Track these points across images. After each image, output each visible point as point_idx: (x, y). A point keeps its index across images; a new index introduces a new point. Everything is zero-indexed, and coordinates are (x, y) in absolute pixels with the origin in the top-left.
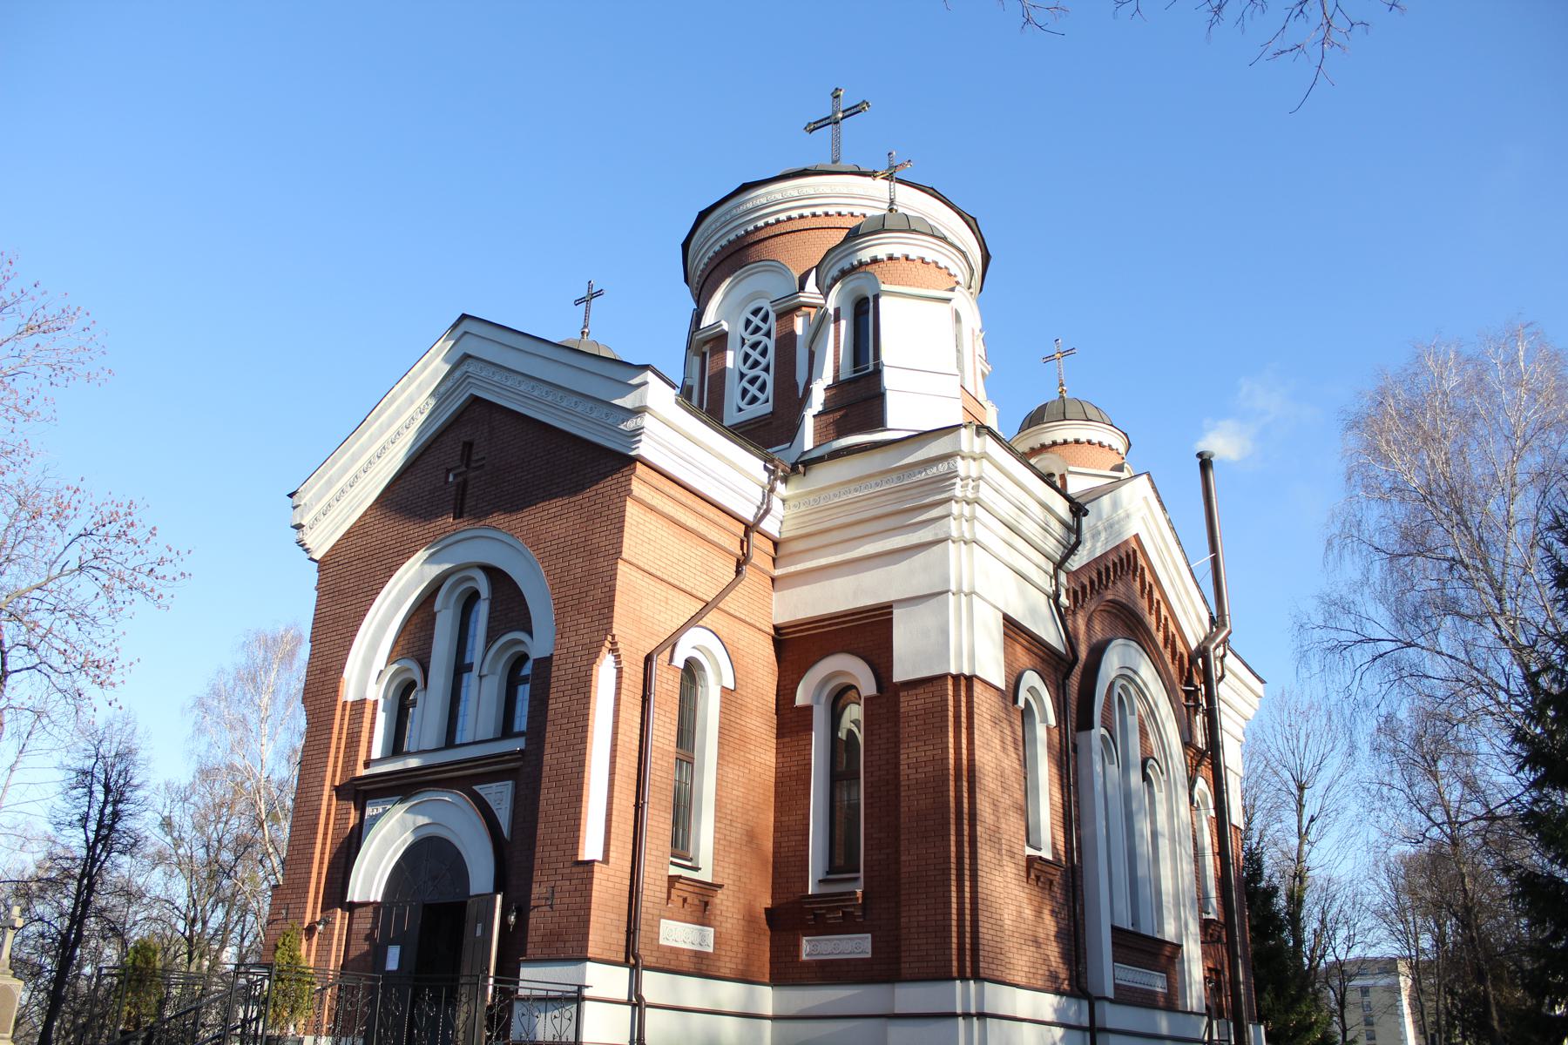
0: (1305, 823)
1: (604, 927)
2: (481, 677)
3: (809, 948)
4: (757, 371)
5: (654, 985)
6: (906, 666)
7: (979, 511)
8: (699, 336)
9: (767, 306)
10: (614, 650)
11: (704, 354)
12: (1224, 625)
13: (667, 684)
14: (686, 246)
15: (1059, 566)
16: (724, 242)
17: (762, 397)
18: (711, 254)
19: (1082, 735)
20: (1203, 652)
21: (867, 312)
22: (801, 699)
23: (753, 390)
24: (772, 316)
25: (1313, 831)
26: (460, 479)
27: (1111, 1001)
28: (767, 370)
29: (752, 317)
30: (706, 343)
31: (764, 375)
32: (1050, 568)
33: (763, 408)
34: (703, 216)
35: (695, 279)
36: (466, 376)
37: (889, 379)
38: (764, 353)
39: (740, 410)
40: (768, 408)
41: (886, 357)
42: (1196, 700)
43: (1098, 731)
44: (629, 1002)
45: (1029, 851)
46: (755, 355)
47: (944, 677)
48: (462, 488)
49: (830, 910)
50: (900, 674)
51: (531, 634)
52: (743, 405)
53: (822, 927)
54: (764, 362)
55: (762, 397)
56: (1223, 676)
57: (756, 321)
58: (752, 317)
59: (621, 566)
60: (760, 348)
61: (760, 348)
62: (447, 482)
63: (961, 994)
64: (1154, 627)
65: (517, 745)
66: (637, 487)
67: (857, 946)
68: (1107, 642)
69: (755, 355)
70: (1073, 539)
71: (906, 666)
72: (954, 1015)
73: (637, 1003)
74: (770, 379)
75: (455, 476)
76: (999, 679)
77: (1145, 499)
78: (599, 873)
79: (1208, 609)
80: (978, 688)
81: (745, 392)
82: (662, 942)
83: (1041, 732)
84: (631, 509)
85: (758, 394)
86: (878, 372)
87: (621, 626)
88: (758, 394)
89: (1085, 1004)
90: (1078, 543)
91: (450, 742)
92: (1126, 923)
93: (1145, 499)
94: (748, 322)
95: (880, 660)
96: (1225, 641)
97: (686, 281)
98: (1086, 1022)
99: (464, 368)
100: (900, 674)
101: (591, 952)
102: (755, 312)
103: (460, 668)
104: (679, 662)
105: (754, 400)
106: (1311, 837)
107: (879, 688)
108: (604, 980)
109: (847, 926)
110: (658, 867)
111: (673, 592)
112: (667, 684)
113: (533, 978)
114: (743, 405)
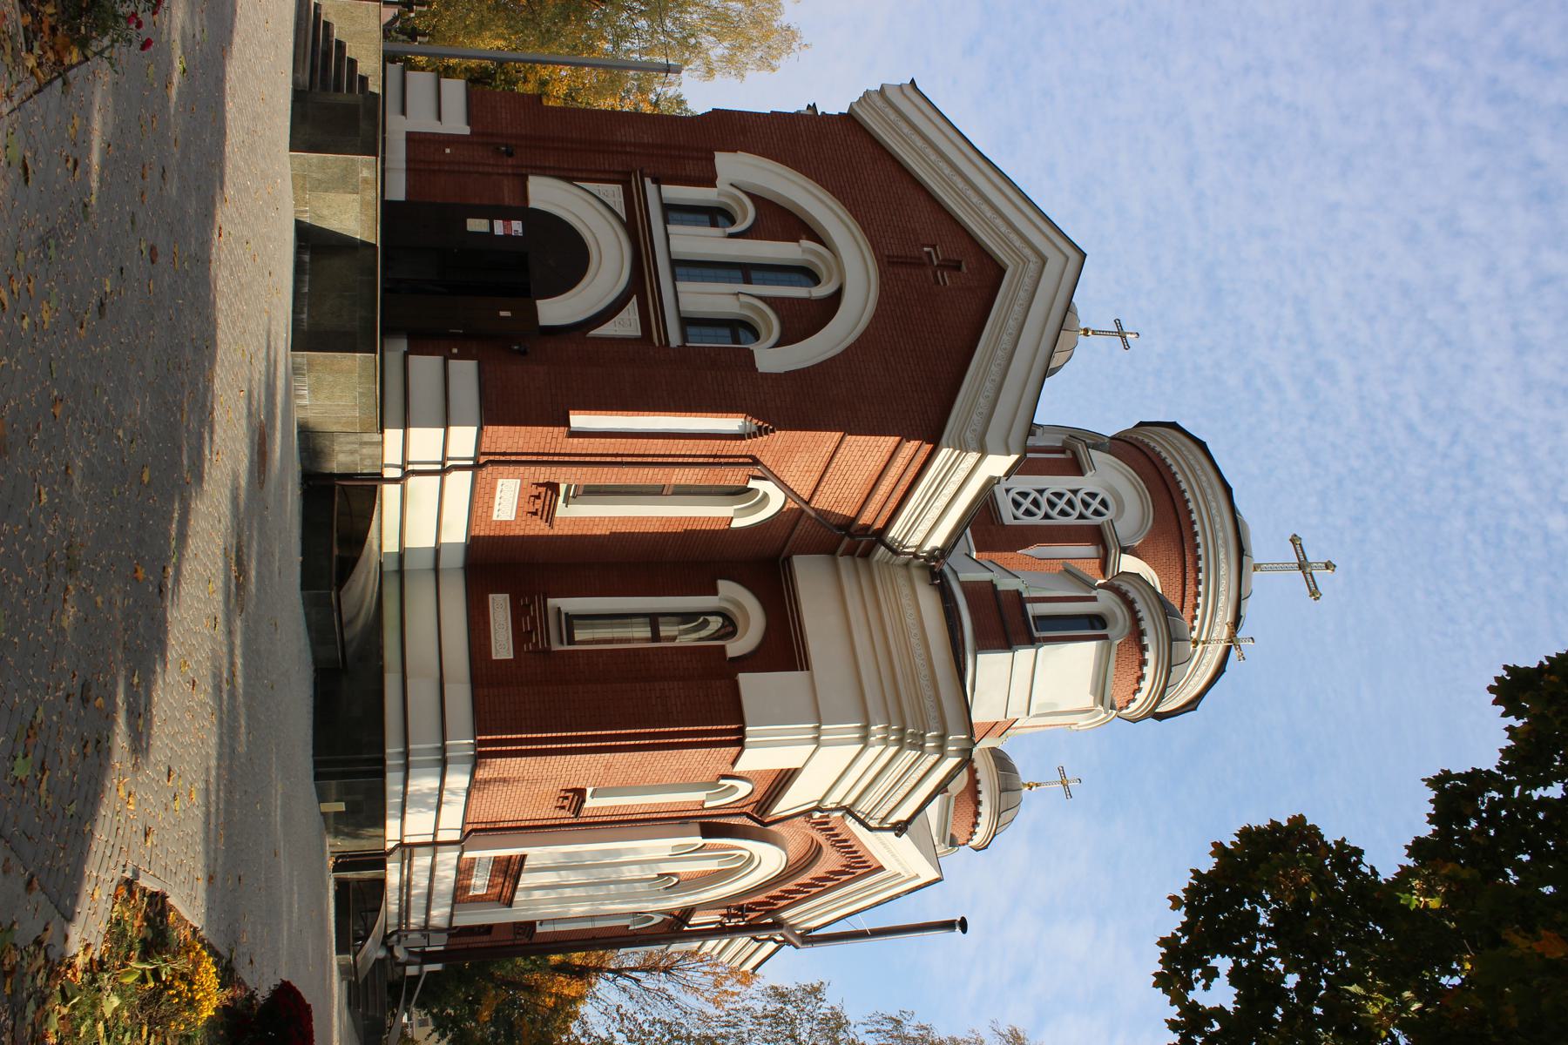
0: (634, 975)
1: (507, 437)
2: (737, 294)
3: (499, 607)
4: (1045, 506)
5: (460, 483)
6: (750, 684)
7: (893, 750)
8: (1081, 448)
9: (1109, 514)
10: (761, 431)
11: (1063, 451)
12: (804, 943)
13: (733, 477)
14: (1174, 426)
15: (849, 811)
16: (1174, 468)
17: (1019, 513)
18: (1164, 454)
19: (697, 828)
20: (778, 925)
21: (1093, 628)
22: (724, 586)
23: (1027, 504)
24: (1097, 520)
25: (626, 983)
26: (926, 259)
27: (460, 857)
28: (1047, 516)
29: (1098, 499)
30: (1074, 453)
31: (1041, 514)
32: (846, 803)
33: (1007, 514)
34: (1202, 446)
35: (1141, 436)
36: (1025, 261)
37: (1024, 655)
38: (1063, 513)
39: (1008, 491)
40: (1008, 519)
41: (1045, 650)
42: (735, 916)
43: (699, 841)
44: (445, 457)
45: (589, 791)
46: (1061, 504)
47: (740, 719)
48: (919, 263)
49: (533, 620)
50: (746, 680)
51: (777, 345)
52: (1012, 494)
53: (518, 613)
54: (1054, 513)
55: (1019, 513)
56: (756, 940)
57: (1095, 504)
58: (1098, 499)
59: (838, 435)
60: (1068, 509)
61: (1068, 509)
62: (924, 245)
63: (461, 743)
64: (799, 881)
65: (675, 339)
66: (910, 447)
67: (502, 647)
68: (784, 848)
69: (1061, 504)
70: (873, 824)
71: (750, 684)
72: (444, 739)
73: (435, 845)
74: (1036, 521)
75: (929, 253)
76: (740, 768)
77: (917, 876)
78: (559, 431)
79: (816, 929)
80: (734, 750)
81: (1025, 495)
82: (500, 481)
83: (699, 796)
84: (892, 441)
85: (1022, 509)
86: (1032, 641)
87: (781, 438)
88: (1022, 509)
89: (456, 836)
90: (870, 829)
91: (675, 264)
92: (528, 864)
93: (917, 876)
94: (1093, 495)
95: (758, 661)
96: (787, 942)
97: (1141, 424)
98: (442, 837)
99: (1033, 258)
100: (746, 680)
101: (489, 429)
102: (1104, 503)
103: (746, 271)
104: (752, 484)
105: (1017, 504)
106: (620, 981)
107: (732, 659)
108: (463, 440)
109: (520, 636)
110: (566, 478)
111: (817, 476)
112: (733, 477)
113: (465, 372)
114: (1012, 494)
